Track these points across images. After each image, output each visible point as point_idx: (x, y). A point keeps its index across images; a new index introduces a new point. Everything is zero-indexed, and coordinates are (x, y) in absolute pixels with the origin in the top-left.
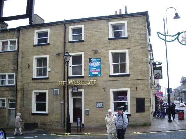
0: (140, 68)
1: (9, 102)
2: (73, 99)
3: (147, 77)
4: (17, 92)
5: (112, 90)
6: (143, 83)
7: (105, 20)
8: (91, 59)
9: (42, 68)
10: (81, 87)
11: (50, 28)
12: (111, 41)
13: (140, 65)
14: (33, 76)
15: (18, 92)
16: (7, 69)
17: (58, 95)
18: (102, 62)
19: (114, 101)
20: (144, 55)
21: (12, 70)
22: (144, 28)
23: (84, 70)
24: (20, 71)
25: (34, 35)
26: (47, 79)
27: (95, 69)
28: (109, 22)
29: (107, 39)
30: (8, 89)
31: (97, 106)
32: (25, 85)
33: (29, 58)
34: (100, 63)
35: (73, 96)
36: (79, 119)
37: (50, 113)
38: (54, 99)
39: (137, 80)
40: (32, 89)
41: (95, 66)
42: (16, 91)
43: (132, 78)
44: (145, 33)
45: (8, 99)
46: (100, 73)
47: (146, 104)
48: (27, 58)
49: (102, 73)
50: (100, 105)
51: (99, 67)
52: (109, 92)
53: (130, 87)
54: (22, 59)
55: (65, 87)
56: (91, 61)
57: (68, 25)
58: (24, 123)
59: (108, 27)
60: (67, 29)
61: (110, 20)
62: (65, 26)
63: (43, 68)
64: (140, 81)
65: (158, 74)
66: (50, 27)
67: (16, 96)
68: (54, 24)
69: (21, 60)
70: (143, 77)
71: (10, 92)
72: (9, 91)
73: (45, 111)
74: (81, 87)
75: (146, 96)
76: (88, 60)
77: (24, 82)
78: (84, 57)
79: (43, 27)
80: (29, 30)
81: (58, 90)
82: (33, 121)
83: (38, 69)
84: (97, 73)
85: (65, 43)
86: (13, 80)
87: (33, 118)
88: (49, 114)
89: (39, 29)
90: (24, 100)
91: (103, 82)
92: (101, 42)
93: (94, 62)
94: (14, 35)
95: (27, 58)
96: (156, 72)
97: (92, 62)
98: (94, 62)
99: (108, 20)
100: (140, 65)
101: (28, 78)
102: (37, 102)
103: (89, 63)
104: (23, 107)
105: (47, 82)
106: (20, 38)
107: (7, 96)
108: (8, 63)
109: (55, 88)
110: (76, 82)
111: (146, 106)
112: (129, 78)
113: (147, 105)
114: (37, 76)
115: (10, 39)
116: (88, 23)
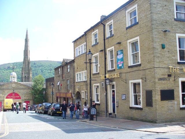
3: (153, 66)
5: (131, 81)
8: (117, 52)
11: (98, 29)
12: (128, 30)
19: (182, 92)
26: (140, 65)
27: (120, 61)
29: (91, 46)
44: (150, 12)
46: (123, 65)
49: (124, 65)
50: (124, 98)
51: (122, 59)
70: (151, 66)
75: (153, 89)
85: (104, 40)
112: (141, 68)
113: (154, 98)
114: (134, 63)
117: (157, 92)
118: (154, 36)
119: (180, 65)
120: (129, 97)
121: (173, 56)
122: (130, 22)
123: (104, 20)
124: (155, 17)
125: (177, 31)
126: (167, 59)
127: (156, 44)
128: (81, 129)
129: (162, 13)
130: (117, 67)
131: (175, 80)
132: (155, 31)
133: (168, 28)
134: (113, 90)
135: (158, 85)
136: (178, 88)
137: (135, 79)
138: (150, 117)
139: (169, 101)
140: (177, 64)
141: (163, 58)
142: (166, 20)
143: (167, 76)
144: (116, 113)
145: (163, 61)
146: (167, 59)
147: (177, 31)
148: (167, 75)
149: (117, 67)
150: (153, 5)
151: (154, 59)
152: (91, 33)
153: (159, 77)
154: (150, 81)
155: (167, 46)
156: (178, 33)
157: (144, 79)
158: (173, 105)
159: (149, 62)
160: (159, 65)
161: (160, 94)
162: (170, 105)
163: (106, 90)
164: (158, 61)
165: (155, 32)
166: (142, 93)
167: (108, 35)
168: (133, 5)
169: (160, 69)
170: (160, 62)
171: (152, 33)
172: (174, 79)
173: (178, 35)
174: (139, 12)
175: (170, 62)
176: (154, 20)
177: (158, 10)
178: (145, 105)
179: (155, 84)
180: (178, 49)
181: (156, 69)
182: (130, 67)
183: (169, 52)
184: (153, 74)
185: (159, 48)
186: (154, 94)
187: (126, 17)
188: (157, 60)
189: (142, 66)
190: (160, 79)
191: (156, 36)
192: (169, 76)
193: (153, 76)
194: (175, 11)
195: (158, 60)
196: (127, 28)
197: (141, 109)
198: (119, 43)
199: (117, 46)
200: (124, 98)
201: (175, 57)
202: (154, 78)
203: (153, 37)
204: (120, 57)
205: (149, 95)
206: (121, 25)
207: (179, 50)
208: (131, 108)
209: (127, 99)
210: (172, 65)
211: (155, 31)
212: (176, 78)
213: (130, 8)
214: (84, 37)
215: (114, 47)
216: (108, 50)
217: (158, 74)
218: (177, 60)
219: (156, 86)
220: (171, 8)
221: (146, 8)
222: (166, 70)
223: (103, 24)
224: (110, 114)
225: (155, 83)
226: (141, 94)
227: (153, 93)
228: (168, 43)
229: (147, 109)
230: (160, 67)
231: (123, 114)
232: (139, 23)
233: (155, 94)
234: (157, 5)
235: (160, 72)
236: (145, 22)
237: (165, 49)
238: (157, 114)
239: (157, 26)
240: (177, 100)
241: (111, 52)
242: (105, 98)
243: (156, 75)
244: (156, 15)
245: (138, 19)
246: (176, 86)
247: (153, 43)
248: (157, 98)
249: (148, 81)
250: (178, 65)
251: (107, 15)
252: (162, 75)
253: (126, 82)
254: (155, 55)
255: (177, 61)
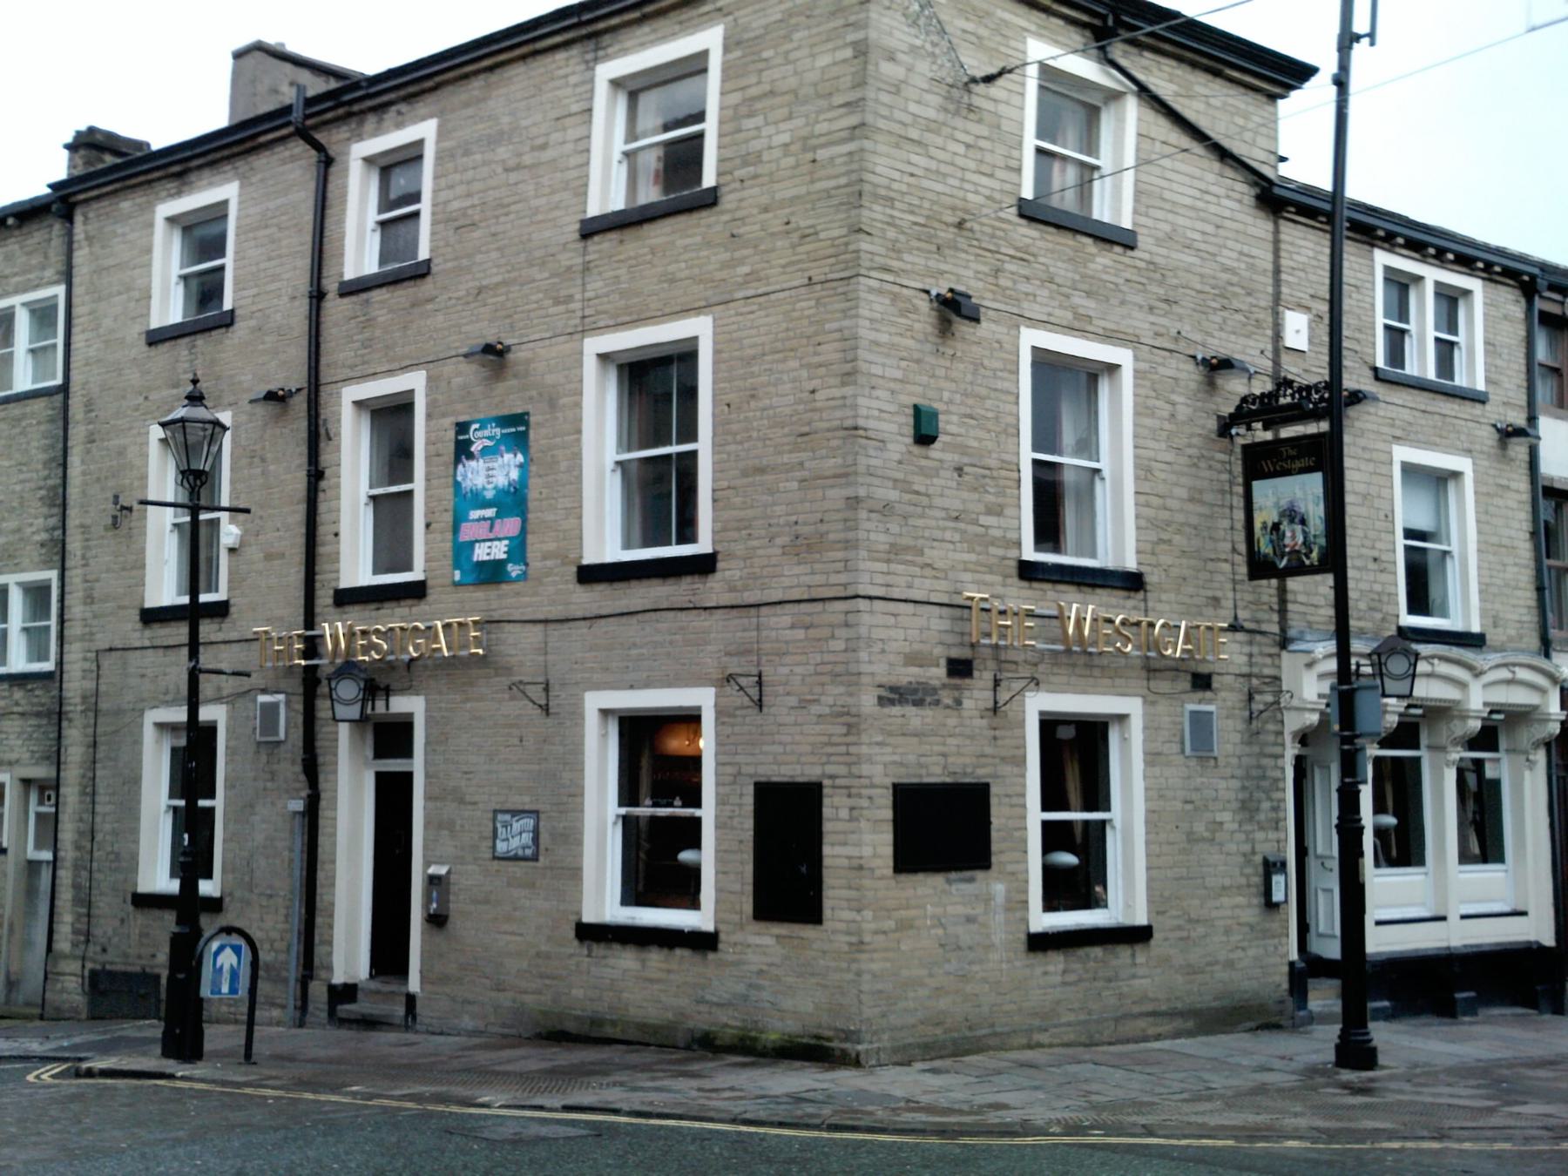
0: (795, 485)
1: (33, 807)
2: (381, 778)
3: (842, 578)
4: (65, 724)
5: (595, 701)
6: (812, 633)
7: (575, 51)
8: (462, 428)
9: (668, 457)
10: (406, 674)
12: (603, 244)
13: (795, 457)
14: (585, 554)
15: (70, 720)
16: (11, 538)
17: (279, 743)
18: (533, 450)
20: (830, 352)
21: (42, 545)
22: (847, 81)
23: (428, 526)
24: (79, 553)
25: (148, 250)
26: (704, 565)
27: (490, 512)
28: (596, 60)
29: (135, 332)
30: (17, 704)
31: (501, 847)
32: (107, 662)
33: (125, 448)
34: (520, 458)
35: (379, 754)
36: (1190, 1024)
37: (231, 894)
38: (255, 779)
39: (764, 610)
40: (143, 700)
41: (489, 494)
42: (58, 715)
43: (732, 589)
44: (853, 120)
45: (27, 783)
46: (518, 549)
47: (827, 839)
48: (115, 442)
49: (530, 555)
50: (516, 838)
51: (513, 501)
52: (578, 715)
53: (716, 675)
54: (88, 452)
55: (318, 682)
56: (469, 443)
57: (341, 133)
58: (87, 973)
59: (590, 110)
60: (333, 169)
61: (606, 39)
62: (318, 147)
63: (679, 455)
64: (787, 620)
65: (1285, 526)
66: (241, 164)
67: (56, 757)
68: (262, 139)
69: (83, 462)
70: (807, 580)
71: (33, 721)
72: (22, 714)
73: (694, 903)
74: (406, 674)
75: (830, 769)
76: (451, 434)
77: (102, 642)
78: (429, 416)
79: (193, 177)
80: (125, 205)
81: (275, 706)
82: (140, 957)
83: (634, 468)
84: (499, 551)
85: (317, 296)
86: (48, 628)
87: (141, 935)
88: (227, 900)
89: (179, 193)
90: (101, 789)
91: (540, 627)
92: (530, 264)
93: (485, 451)
94: (46, 257)
95: (115, 442)
96: (1270, 502)
97: (470, 456)
98: (485, 451)
99: (591, 44)
100: (795, 457)
101: (120, 607)
102: (644, 811)
103: (457, 461)
104: (88, 845)
105: (220, 637)
106: (76, 280)
107: (13, 756)
108: (18, 488)
109: (264, 691)
110: (364, 633)
111: (826, 862)
112: (713, 589)
113: (838, 850)
115: (25, 291)
116: (464, 97)
117: (865, 803)
118: (865, 333)
119: (1035, 585)
120: (572, 838)
121: (991, 511)
122: (624, 168)
123: (301, 112)
124: (885, 165)
125: (1025, 305)
126: (944, 529)
127: (875, 404)
128: (666, 1083)
129: (939, 141)
130: (457, 565)
131: (995, 709)
132: (871, 290)
133: (965, 276)
134: (394, 765)
135: (879, 738)
136: (1016, 770)
137: (647, 684)
138: (794, 1009)
139: (953, 875)
140: (1015, 580)
141: (920, 522)
142: (959, 203)
143: (939, 673)
144: (414, 984)
145: (920, 542)
146: (944, 529)
147: (1025, 305)
148: (943, 662)
149: (457, 565)
150: (887, 68)
151: (851, 524)
152: (150, 208)
153: (884, 680)
154: (803, 704)
155: (949, 425)
156: (1034, 323)
157: (750, 691)
158: (979, 910)
159: (803, 546)
160: (890, 579)
161: (888, 814)
162: (960, 910)
163: (311, 767)
164: (881, 540)
165: (873, 305)
166: (721, 801)
167: (360, 255)
168: (687, 28)
169: (891, 606)
170: (895, 552)
171: (850, 299)
172: (990, 694)
173: (1032, 338)
174: (735, 98)
175: (966, 557)
176: (876, 196)
177: (913, 107)
178: (748, 907)
179: (851, 728)
180: (1027, 455)
181: (862, 604)
182: (590, 575)
183: (959, 470)
184: (839, 645)
185: (898, 430)
186: (844, 814)
187: (589, 122)
188: (874, 533)
189: (728, 569)
190: (896, 695)
191: (873, 335)
192: (960, 668)
193: (839, 669)
194: (1030, 141)
195: (882, 538)
196: (591, 230)
197: (703, 942)
198: (494, 353)
199: (467, 374)
200: (515, 843)
201: (1003, 522)
202: (850, 678)
203: (849, 343)
204: (493, 472)
205: (788, 827)
206: (529, 189)
207: (1036, 462)
208: (592, 934)
209: (552, 853)
210: (981, 585)
211: (871, 290)
212: (1003, 696)
213: (643, 46)
214: (49, 235)
215: (429, 379)
216: (347, 402)
217: (878, 647)
218: (1018, 544)
219: (864, 750)
220: (1002, 109)
221: (812, 77)
222: (937, 622)
223: (318, 147)
224: (347, 992)
225: (852, 723)
226: (707, 813)
227: (834, 809)
228: (958, 398)
229: (766, 943)
230: (896, 594)
231: (499, 988)
232: (728, 201)
233: (851, 820)
234: (910, 69)
235: (892, 633)
236: (794, 200)
237: (935, 451)
238: (865, 987)
239: (895, 250)
240: (1010, 868)
241: (391, 417)
242: (290, 846)
243: (863, 655)
244: (893, 151)
245: (721, 161)
246: (1003, 759)
247: (848, 391)
248: (867, 851)
249: (780, 706)
250: (1025, 584)
251: (370, 65)
252: (912, 659)
253: (550, 702)
254: (862, 492)
255: (1013, 553)
